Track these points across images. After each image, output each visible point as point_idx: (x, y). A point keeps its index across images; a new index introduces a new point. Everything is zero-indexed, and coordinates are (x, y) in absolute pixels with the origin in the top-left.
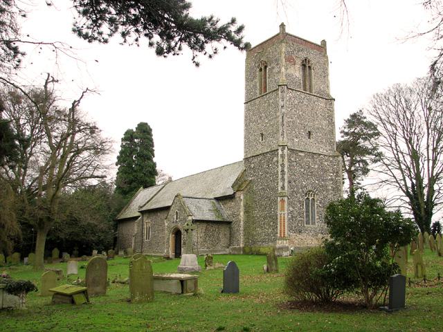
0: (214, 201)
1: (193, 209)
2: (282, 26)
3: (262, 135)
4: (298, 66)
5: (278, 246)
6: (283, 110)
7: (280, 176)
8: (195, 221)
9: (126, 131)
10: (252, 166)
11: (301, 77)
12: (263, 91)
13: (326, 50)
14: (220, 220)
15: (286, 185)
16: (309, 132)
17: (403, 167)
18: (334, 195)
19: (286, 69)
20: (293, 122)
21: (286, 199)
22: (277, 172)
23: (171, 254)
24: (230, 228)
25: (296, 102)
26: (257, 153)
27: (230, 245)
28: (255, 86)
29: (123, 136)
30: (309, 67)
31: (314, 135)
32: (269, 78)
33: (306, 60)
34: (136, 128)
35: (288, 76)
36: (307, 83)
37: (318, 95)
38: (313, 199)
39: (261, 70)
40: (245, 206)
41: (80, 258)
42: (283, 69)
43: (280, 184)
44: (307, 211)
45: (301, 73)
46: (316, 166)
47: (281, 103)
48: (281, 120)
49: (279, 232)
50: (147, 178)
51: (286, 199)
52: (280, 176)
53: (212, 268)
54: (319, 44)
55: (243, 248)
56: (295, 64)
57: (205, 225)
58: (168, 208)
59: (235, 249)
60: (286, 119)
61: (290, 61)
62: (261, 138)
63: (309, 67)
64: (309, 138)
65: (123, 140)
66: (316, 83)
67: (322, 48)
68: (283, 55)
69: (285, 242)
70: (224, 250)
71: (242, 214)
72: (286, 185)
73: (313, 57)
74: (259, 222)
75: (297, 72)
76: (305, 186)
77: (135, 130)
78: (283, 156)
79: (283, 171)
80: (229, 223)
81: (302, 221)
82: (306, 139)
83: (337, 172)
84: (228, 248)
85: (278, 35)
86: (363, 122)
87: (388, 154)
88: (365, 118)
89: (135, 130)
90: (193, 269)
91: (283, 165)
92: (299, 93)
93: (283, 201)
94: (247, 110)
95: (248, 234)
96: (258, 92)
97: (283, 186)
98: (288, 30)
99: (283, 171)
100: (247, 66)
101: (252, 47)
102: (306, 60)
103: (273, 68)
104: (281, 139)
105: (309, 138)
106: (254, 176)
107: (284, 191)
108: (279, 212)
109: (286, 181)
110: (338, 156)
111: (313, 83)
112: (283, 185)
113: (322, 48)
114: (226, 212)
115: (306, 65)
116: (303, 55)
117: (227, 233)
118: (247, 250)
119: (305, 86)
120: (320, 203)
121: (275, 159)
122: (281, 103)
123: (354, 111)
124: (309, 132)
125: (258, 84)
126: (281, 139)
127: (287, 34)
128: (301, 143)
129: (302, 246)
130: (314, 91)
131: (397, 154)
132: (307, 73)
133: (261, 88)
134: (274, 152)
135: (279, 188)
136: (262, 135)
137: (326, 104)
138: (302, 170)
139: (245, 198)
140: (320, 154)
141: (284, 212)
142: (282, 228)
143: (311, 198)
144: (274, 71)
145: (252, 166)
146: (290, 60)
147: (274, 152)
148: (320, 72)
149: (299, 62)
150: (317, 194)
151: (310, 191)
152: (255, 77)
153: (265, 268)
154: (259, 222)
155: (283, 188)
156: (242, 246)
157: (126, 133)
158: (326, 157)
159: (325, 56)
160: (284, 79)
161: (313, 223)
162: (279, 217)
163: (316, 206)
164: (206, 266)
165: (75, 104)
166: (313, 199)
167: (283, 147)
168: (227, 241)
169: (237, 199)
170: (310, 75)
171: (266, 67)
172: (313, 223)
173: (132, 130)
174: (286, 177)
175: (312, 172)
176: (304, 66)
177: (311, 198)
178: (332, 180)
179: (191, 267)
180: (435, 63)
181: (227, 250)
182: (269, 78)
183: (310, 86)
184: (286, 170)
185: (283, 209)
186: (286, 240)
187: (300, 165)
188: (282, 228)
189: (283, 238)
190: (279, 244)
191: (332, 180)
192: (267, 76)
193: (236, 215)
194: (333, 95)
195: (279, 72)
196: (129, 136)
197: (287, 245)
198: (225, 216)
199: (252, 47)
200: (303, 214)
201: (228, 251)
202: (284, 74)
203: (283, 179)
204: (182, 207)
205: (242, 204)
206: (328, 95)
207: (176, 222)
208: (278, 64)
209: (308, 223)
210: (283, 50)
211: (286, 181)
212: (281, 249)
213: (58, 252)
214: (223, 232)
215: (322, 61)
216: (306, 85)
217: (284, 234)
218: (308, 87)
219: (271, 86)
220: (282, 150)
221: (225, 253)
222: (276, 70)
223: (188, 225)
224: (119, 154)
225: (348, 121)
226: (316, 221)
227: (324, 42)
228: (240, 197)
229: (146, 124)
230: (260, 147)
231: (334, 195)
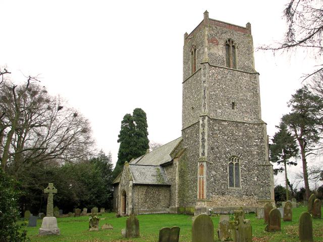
0: (159, 168)
1: (136, 174)
2: (206, 13)
3: (193, 108)
4: (221, 45)
6: (205, 85)
8: (135, 185)
9: (125, 115)
13: (250, 31)
14: (160, 183)
16: (233, 103)
18: (259, 160)
19: (209, 49)
20: (216, 95)
22: (208, 140)
24: (170, 191)
25: (220, 77)
27: (169, 205)
28: (189, 67)
29: (123, 120)
30: (233, 47)
34: (134, 113)
36: (231, 61)
37: (242, 70)
39: (192, 53)
40: (180, 171)
41: (67, 215)
42: (206, 49)
43: (201, 151)
45: (225, 52)
46: (241, 134)
49: (198, 194)
50: (140, 152)
51: (205, 164)
53: (96, 229)
54: (245, 26)
55: (178, 208)
56: (218, 45)
57: (146, 188)
59: (172, 209)
60: (207, 92)
61: (212, 42)
63: (233, 46)
64: (233, 108)
65: (122, 122)
66: (240, 60)
67: (246, 30)
69: (203, 203)
70: (166, 210)
71: (177, 178)
73: (237, 38)
75: (220, 51)
76: (229, 152)
77: (132, 114)
79: (203, 139)
80: (169, 186)
81: (225, 183)
82: (230, 110)
84: (168, 208)
86: (309, 96)
88: (310, 92)
89: (132, 114)
90: (50, 232)
91: (203, 134)
93: (202, 166)
94: (184, 88)
95: (182, 196)
98: (211, 16)
99: (203, 139)
100: (184, 52)
102: (229, 40)
104: (203, 110)
105: (233, 108)
106: (188, 145)
107: (203, 157)
111: (237, 60)
112: (204, 152)
113: (246, 30)
116: (226, 37)
117: (167, 194)
118: (182, 210)
120: (245, 167)
123: (300, 87)
124: (233, 103)
126: (203, 110)
127: (209, 19)
128: (224, 113)
129: (225, 207)
130: (238, 67)
132: (231, 52)
133: (192, 69)
135: (200, 155)
136: (193, 108)
137: (250, 77)
138: (226, 137)
139: (180, 164)
143: (234, 163)
146: (213, 41)
151: (234, 156)
155: (203, 154)
156: (176, 206)
157: (125, 117)
158: (251, 126)
159: (250, 36)
160: (207, 57)
161: (237, 186)
162: (198, 180)
163: (240, 169)
164: (90, 227)
167: (204, 117)
168: (167, 201)
169: (175, 165)
170: (234, 52)
172: (237, 186)
173: (130, 114)
174: (206, 144)
175: (236, 139)
176: (227, 46)
177: (234, 163)
178: (257, 145)
179: (48, 230)
180: (290, 6)
184: (206, 138)
185: (202, 173)
186: (204, 201)
187: (223, 133)
191: (257, 145)
193: (173, 179)
194: (257, 69)
195: (203, 52)
196: (127, 119)
197: (205, 206)
201: (168, 210)
202: (207, 54)
203: (203, 146)
206: (253, 70)
209: (232, 185)
213: (97, 208)
214: (163, 195)
216: (230, 62)
217: (203, 196)
218: (232, 64)
220: (203, 120)
221: (165, 212)
222: (202, 51)
224: (120, 134)
225: (295, 96)
226: (241, 183)
227: (249, 25)
229: (140, 109)
231: (259, 160)
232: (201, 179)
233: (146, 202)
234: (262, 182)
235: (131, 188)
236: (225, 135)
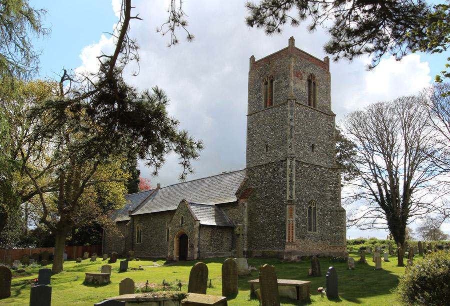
4: (305, 81)
5: (286, 250)
6: (292, 123)
7: (288, 186)
10: (256, 175)
11: (307, 93)
12: (268, 104)
15: (294, 194)
16: (313, 145)
17: (380, 181)
18: (333, 205)
19: (295, 83)
20: (299, 135)
21: (294, 207)
23: (175, 255)
25: (302, 117)
26: (261, 163)
27: (232, 249)
28: (260, 99)
30: (314, 83)
31: (316, 149)
32: (275, 92)
33: (311, 75)
35: (296, 90)
38: (315, 208)
39: (266, 83)
40: (249, 213)
42: (292, 84)
43: (288, 193)
44: (310, 220)
45: (307, 88)
47: (290, 116)
48: (290, 132)
52: (288, 186)
58: (172, 212)
60: (294, 132)
61: (298, 76)
62: (265, 149)
64: (313, 151)
68: (292, 70)
71: (245, 220)
72: (294, 194)
73: (317, 72)
74: (263, 228)
78: (291, 167)
79: (291, 181)
82: (309, 152)
83: (336, 184)
84: (230, 251)
85: (286, 49)
87: (365, 168)
91: (291, 176)
92: (304, 108)
93: (291, 209)
94: (248, 120)
96: (263, 105)
97: (290, 193)
98: (297, 45)
99: (291, 181)
101: (256, 60)
102: (311, 75)
103: (280, 82)
104: (289, 151)
105: (313, 151)
108: (288, 219)
109: (294, 190)
110: (337, 169)
112: (292, 194)
114: (229, 218)
115: (311, 81)
116: (309, 70)
117: (230, 237)
119: (310, 101)
120: (321, 211)
121: (281, 169)
122: (290, 116)
124: (313, 145)
125: (263, 97)
127: (295, 48)
131: (374, 169)
134: (281, 163)
139: (248, 206)
140: (321, 167)
141: (292, 219)
142: (291, 234)
143: (313, 207)
144: (281, 85)
145: (256, 175)
147: (281, 163)
148: (323, 88)
149: (305, 77)
150: (318, 204)
152: (259, 91)
153: (310, 271)
154: (263, 228)
165: (110, 69)
166: (315, 208)
170: (315, 91)
171: (272, 82)
174: (294, 186)
175: (314, 183)
176: (309, 81)
178: (331, 190)
181: (230, 253)
182: (275, 92)
183: (314, 102)
184: (294, 180)
185: (291, 216)
186: (294, 245)
188: (291, 234)
189: (292, 243)
190: (288, 248)
192: (274, 89)
198: (228, 220)
199: (256, 60)
200: (306, 221)
203: (291, 188)
204: (189, 213)
205: (246, 210)
206: (330, 111)
207: (182, 226)
208: (286, 79)
209: (310, 230)
210: (293, 64)
211: (294, 190)
212: (290, 253)
214: (226, 239)
215: (325, 77)
219: (278, 99)
222: (284, 84)
223: (239, 230)
226: (317, 228)
228: (243, 204)
230: (264, 158)
232: (291, 222)
233: (211, 245)
234: (335, 228)
235: (197, 230)
236: (306, 179)
